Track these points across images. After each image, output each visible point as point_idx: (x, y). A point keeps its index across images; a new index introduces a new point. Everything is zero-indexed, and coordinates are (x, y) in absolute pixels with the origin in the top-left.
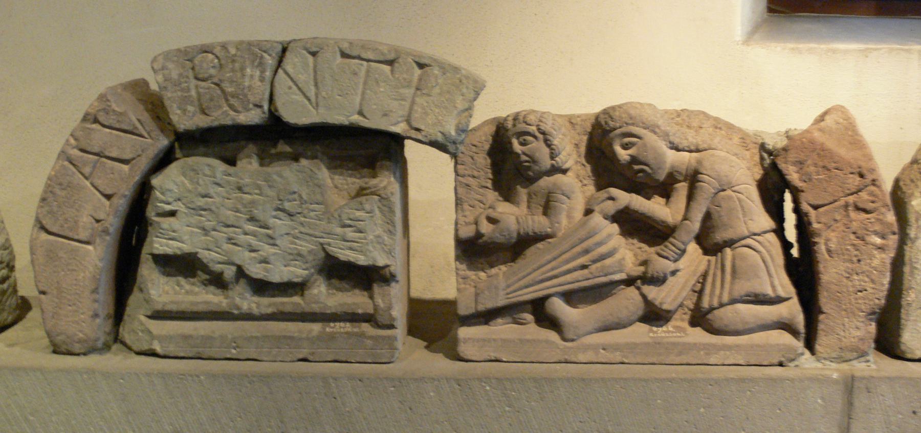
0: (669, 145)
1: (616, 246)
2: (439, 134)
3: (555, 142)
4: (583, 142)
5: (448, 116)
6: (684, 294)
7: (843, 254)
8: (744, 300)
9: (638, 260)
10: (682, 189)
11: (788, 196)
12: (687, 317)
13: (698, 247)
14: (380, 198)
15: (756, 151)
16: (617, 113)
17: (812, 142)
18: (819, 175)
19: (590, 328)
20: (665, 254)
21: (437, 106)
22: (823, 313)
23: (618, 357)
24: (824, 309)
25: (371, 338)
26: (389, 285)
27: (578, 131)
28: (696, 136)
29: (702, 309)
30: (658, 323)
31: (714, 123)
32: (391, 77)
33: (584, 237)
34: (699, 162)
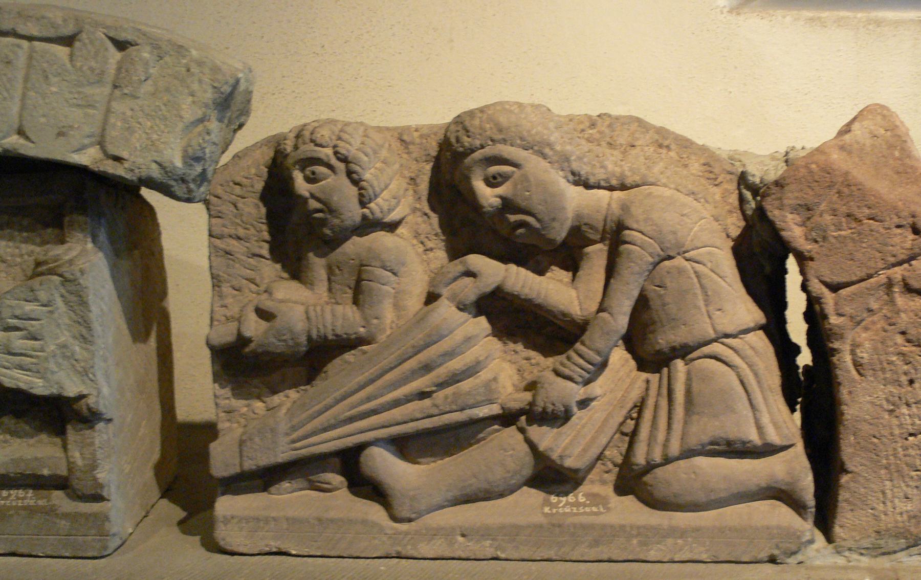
0: (571, 178)
1: (481, 358)
2: (154, 166)
3: (367, 176)
4: (424, 174)
5: (168, 133)
6: (604, 440)
7: (883, 370)
8: (710, 450)
9: (526, 379)
10: (597, 254)
11: (791, 263)
12: (611, 477)
13: (629, 356)
14: (61, 279)
15: (733, 186)
16: (477, 122)
17: (827, 170)
18: (840, 230)
19: (438, 499)
20: (567, 372)
21: (148, 116)
22: (847, 472)
23: (487, 548)
24: (849, 466)
25: (66, 516)
26: (92, 428)
27: (414, 155)
28: (622, 160)
29: (635, 467)
30: (562, 489)
31: (656, 137)
32: (69, 65)
33: (422, 343)
34: (625, 208)
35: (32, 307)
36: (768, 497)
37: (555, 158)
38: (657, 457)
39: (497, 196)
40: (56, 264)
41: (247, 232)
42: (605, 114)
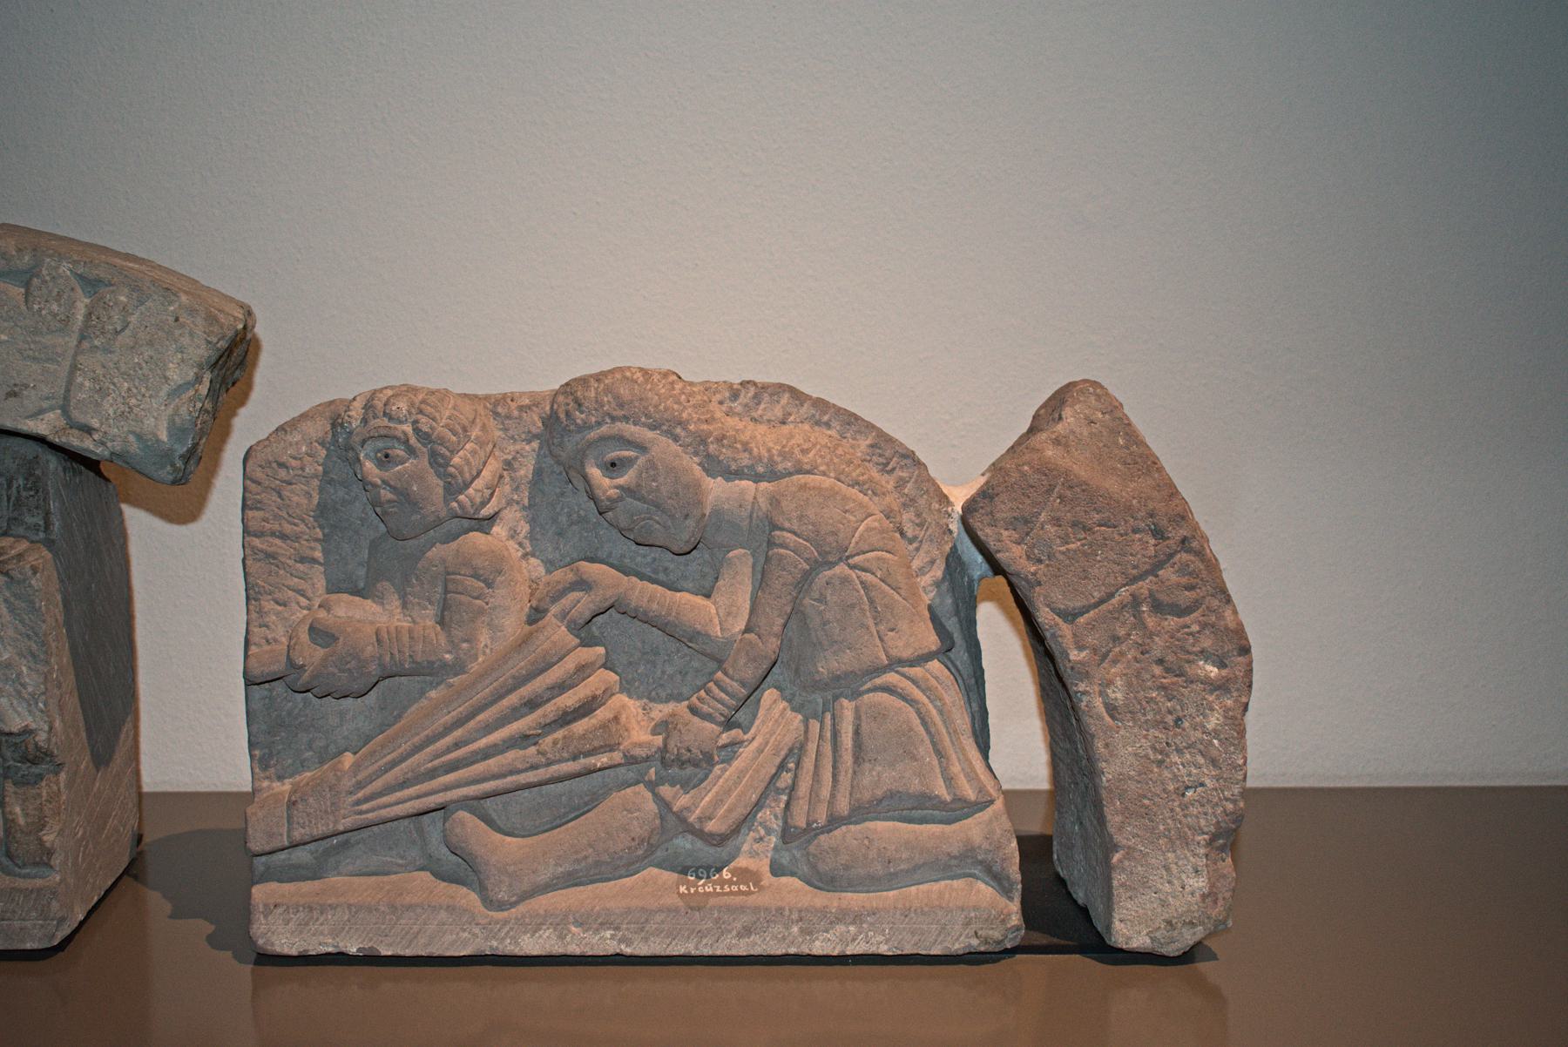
1: (599, 692)
2: (131, 438)
20: (705, 708)
32: (23, 308)
36: (445, 771)
37: (689, 440)
38: (822, 818)
39: (616, 487)
41: (295, 528)
42: (748, 382)
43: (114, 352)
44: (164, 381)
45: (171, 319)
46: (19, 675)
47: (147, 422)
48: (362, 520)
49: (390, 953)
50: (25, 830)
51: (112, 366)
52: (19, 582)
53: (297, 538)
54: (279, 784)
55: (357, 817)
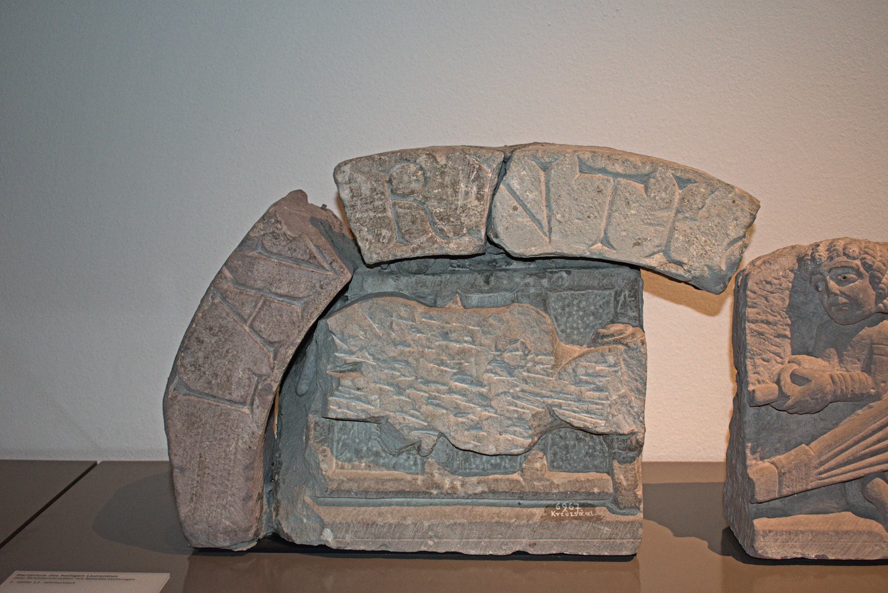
2: (706, 268)
25: (608, 523)
32: (645, 195)
35: (600, 368)
40: (621, 336)
41: (775, 318)
43: (697, 220)
44: (726, 236)
45: (730, 202)
46: (630, 402)
47: (715, 259)
48: (813, 313)
49: (833, 558)
50: (627, 489)
51: (696, 228)
52: (633, 349)
53: (776, 324)
54: (761, 462)
55: (819, 481)
